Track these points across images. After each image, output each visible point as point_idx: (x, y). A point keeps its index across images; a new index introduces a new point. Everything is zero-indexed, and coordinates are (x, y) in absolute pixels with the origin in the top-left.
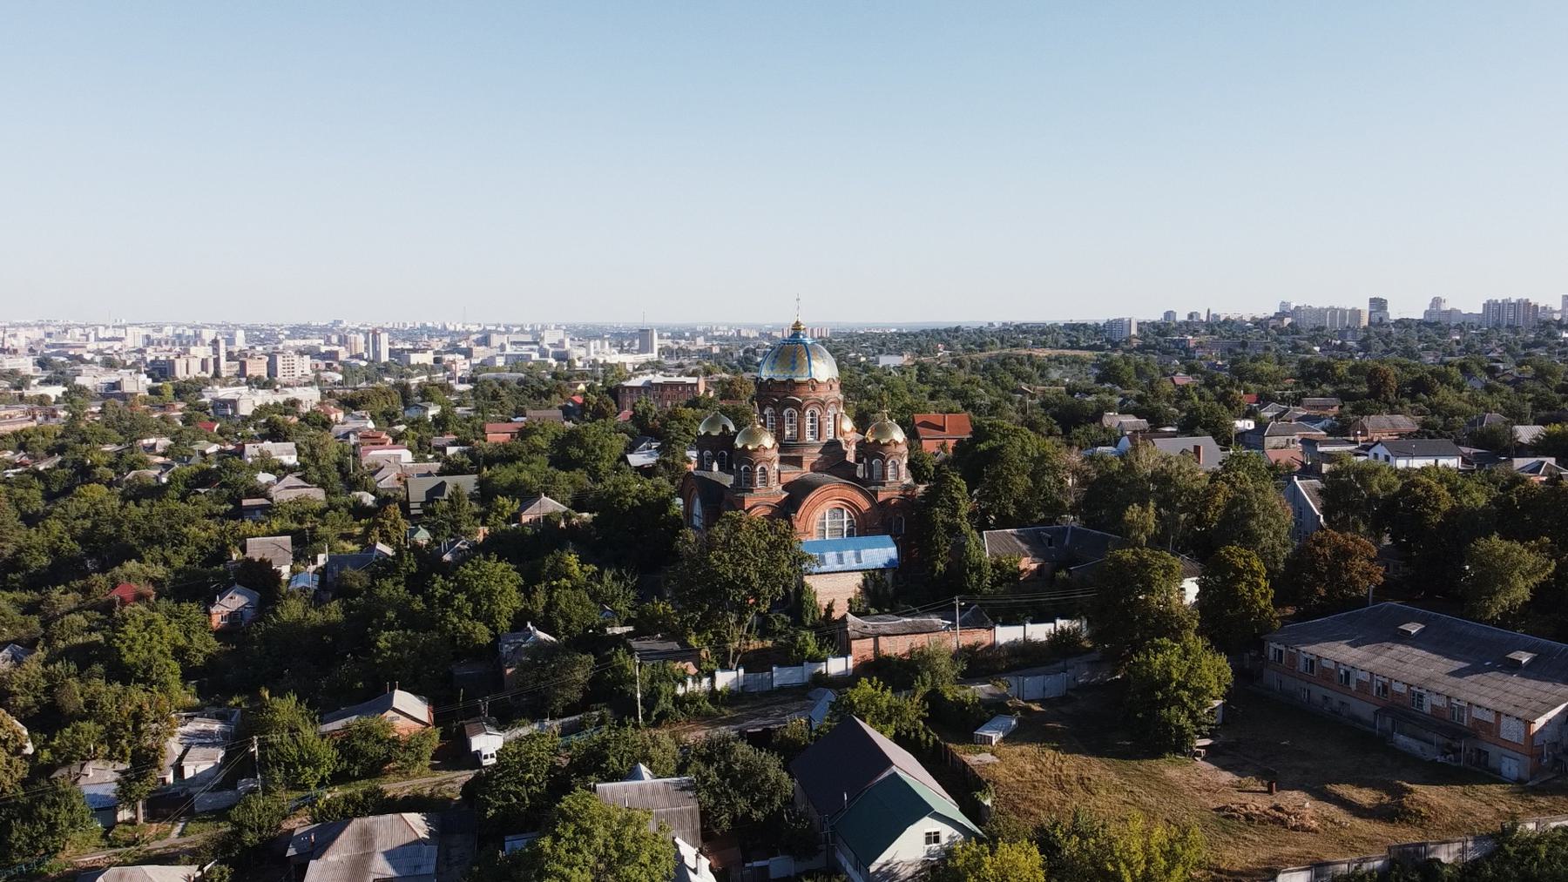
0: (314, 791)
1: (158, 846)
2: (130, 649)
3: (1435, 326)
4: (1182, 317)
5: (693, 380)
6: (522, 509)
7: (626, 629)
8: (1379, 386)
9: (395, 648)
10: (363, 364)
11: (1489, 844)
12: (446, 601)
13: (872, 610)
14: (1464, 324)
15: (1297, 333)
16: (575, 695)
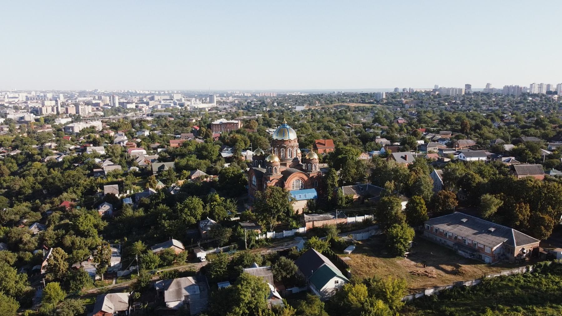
0: (154, 270)
1: (110, 287)
2: (81, 226)
3: (487, 94)
4: (400, 90)
5: (236, 122)
6: (192, 174)
7: (237, 218)
9: (170, 226)
11: (479, 281)
12: (182, 211)
13: (310, 212)
15: (440, 97)
16: (226, 240)
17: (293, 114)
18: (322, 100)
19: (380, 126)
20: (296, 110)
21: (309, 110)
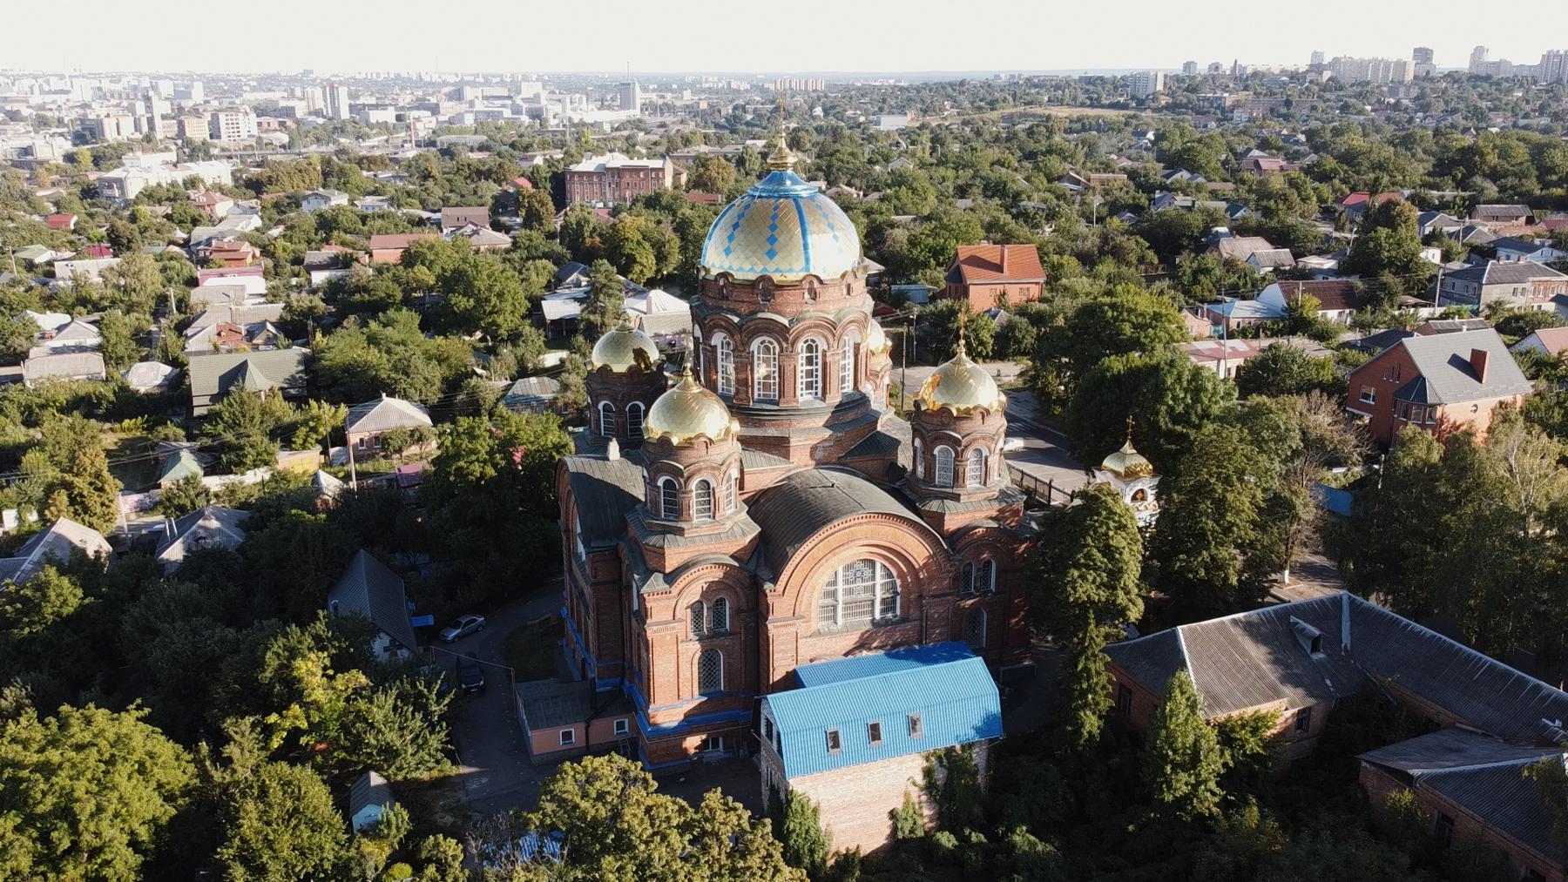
3: (1486, 82)
4: (1202, 68)
6: (353, 418)
10: (321, 121)
14: (1520, 80)
15: (1341, 88)
17: (870, 139)
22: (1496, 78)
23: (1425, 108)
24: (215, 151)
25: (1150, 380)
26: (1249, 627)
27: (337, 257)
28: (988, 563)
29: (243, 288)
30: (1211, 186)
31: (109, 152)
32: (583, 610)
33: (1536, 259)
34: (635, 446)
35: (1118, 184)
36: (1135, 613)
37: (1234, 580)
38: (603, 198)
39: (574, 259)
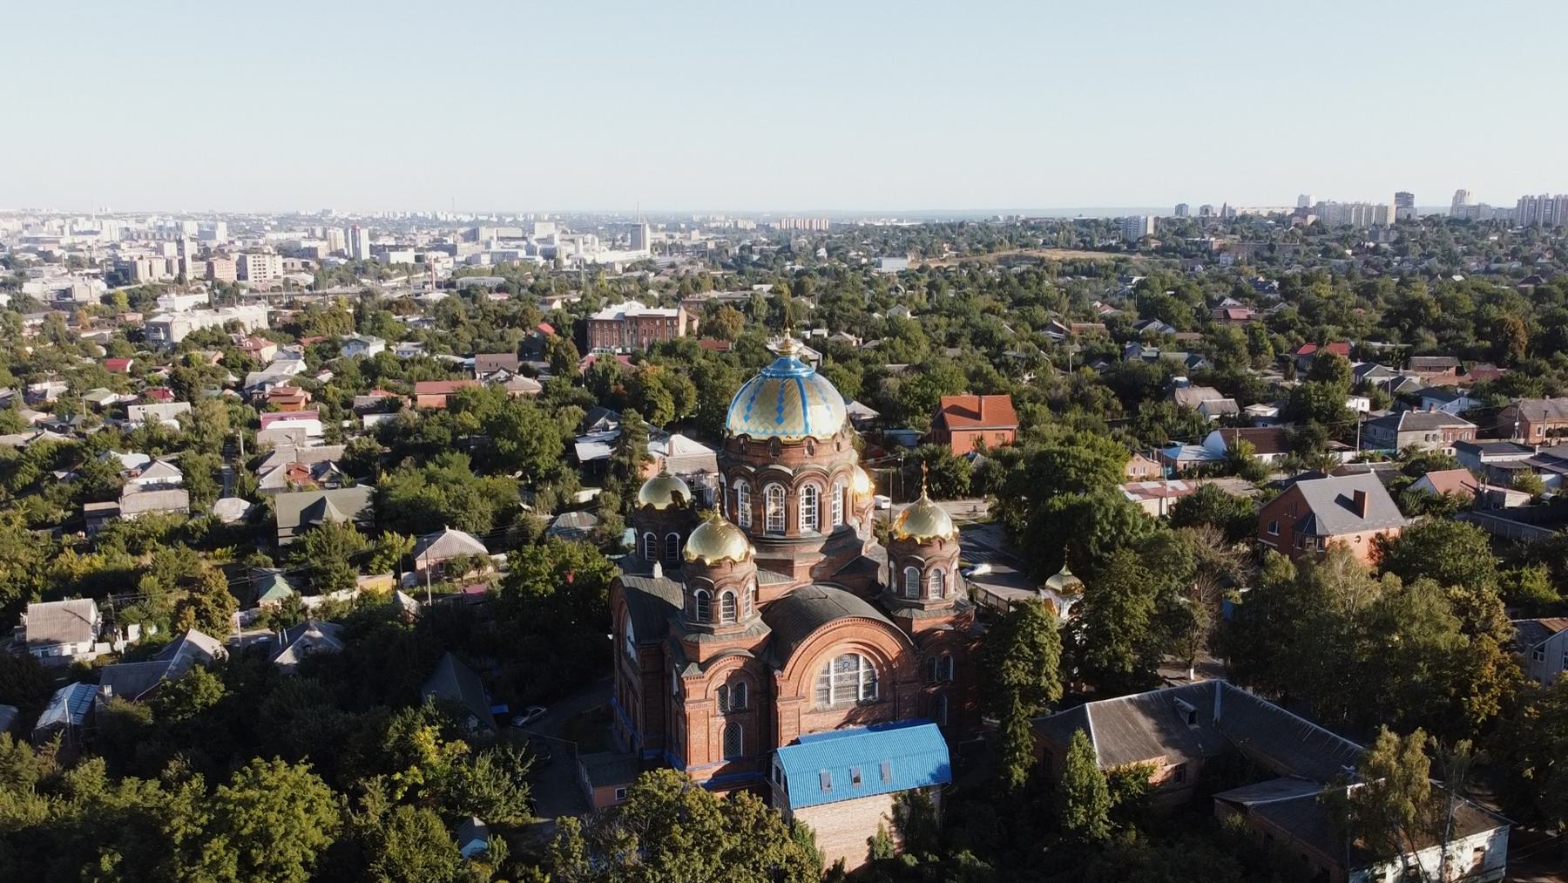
3: (1464, 225)
4: (1194, 211)
5: (672, 313)
6: (418, 550)
8: (1506, 343)
10: (343, 261)
14: (1497, 222)
17: (871, 283)
18: (960, 239)
19: (1171, 330)
20: (883, 270)
21: (922, 269)
22: (1474, 221)
23: (1402, 252)
24: (244, 292)
25: (1081, 517)
26: (1140, 705)
27: (383, 401)
28: (947, 658)
29: (303, 430)
30: (1180, 336)
31: (144, 294)
32: (631, 696)
33: (1452, 408)
34: (677, 568)
35: (1095, 334)
36: (1056, 694)
37: (1130, 669)
38: (621, 343)
39: (600, 404)
